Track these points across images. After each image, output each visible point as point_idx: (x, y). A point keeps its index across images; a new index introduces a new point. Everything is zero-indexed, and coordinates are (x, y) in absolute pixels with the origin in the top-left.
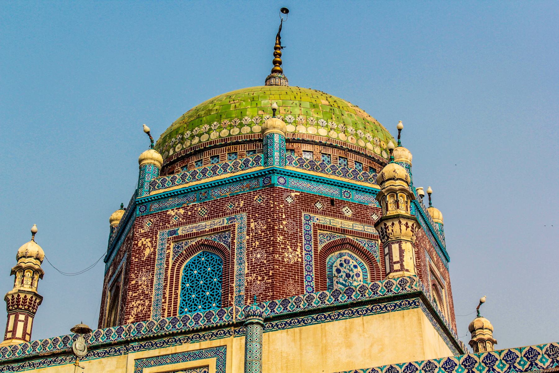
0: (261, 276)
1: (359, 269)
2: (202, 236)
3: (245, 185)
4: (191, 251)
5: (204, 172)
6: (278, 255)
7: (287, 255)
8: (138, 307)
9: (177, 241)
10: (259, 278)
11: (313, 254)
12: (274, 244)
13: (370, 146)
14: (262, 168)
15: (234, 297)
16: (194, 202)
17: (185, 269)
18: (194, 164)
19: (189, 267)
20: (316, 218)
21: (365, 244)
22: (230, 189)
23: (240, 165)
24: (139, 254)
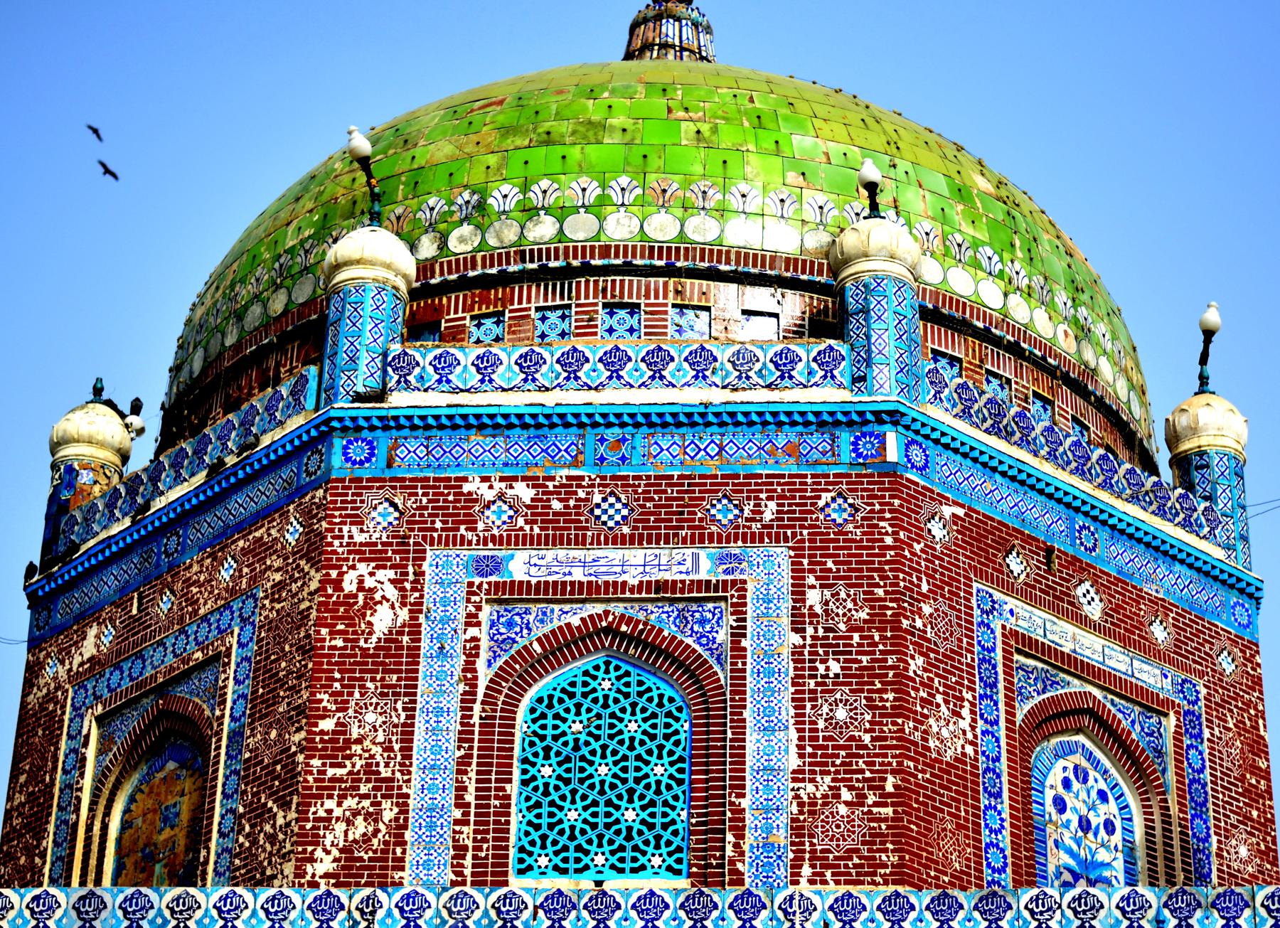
0: (851, 788)
1: (1112, 807)
2: (609, 601)
3: (781, 441)
4: (562, 646)
5: (614, 362)
6: (911, 724)
7: (935, 729)
8: (349, 822)
9: (507, 601)
10: (846, 795)
11: (1002, 733)
12: (901, 682)
13: (1106, 370)
14: (845, 395)
15: (746, 848)
16: (575, 463)
17: (533, 710)
18: (532, 312)
19: (550, 706)
20: (1007, 608)
21: (1133, 722)
22: (721, 448)
23: (758, 366)
24: (349, 619)
